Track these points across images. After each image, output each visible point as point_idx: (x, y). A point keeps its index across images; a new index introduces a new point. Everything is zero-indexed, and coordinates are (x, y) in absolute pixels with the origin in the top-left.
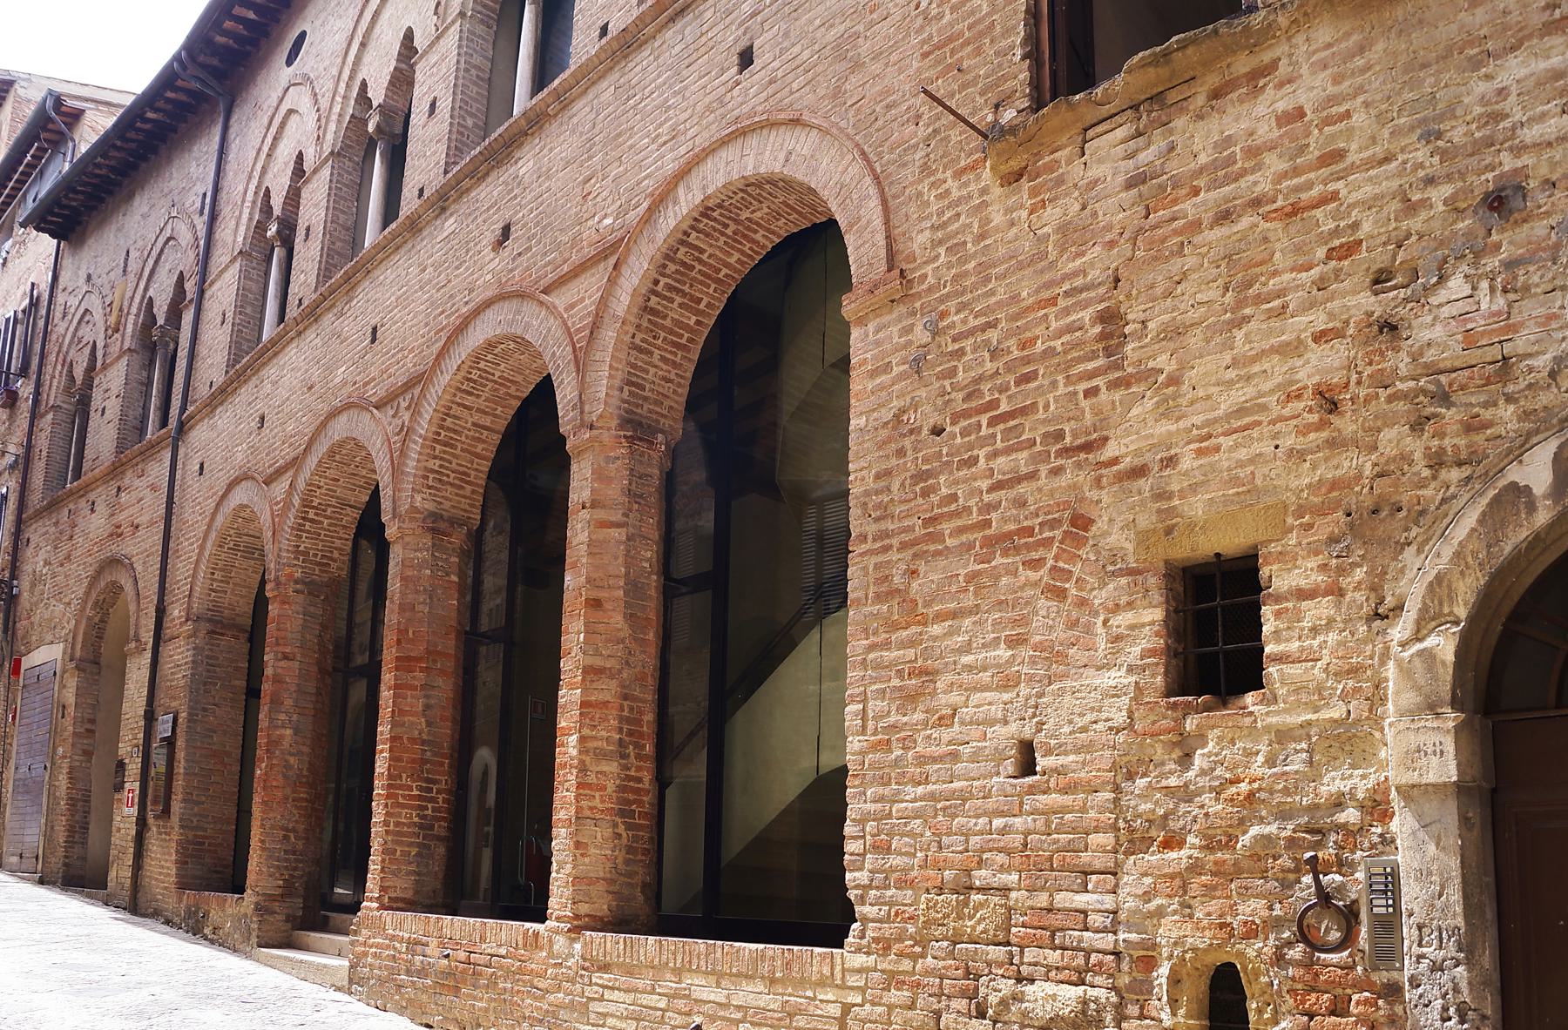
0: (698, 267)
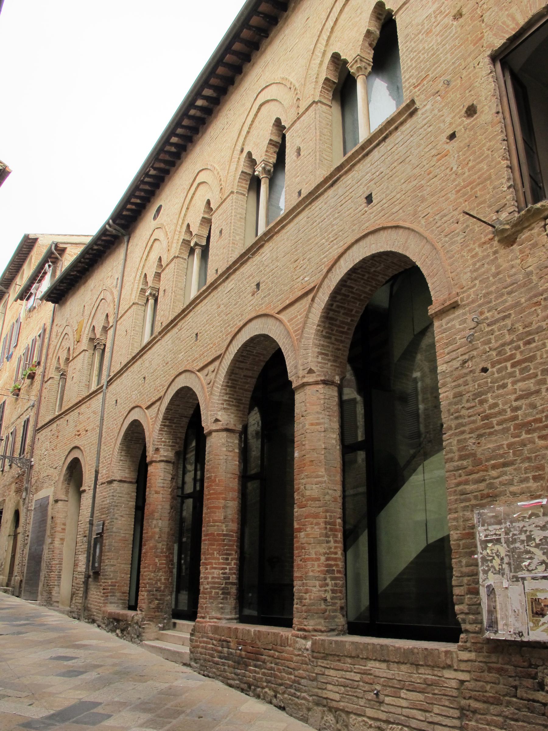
0: (351, 295)
